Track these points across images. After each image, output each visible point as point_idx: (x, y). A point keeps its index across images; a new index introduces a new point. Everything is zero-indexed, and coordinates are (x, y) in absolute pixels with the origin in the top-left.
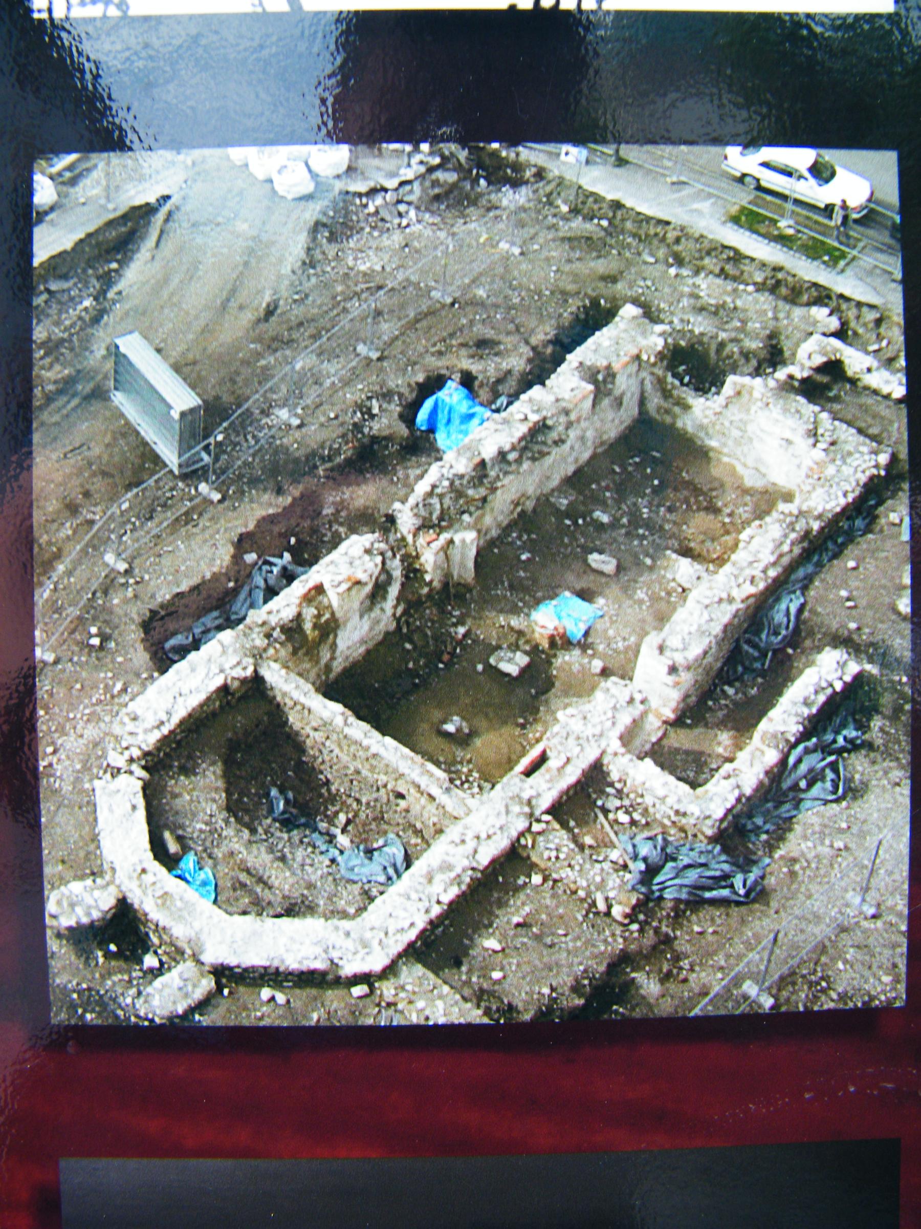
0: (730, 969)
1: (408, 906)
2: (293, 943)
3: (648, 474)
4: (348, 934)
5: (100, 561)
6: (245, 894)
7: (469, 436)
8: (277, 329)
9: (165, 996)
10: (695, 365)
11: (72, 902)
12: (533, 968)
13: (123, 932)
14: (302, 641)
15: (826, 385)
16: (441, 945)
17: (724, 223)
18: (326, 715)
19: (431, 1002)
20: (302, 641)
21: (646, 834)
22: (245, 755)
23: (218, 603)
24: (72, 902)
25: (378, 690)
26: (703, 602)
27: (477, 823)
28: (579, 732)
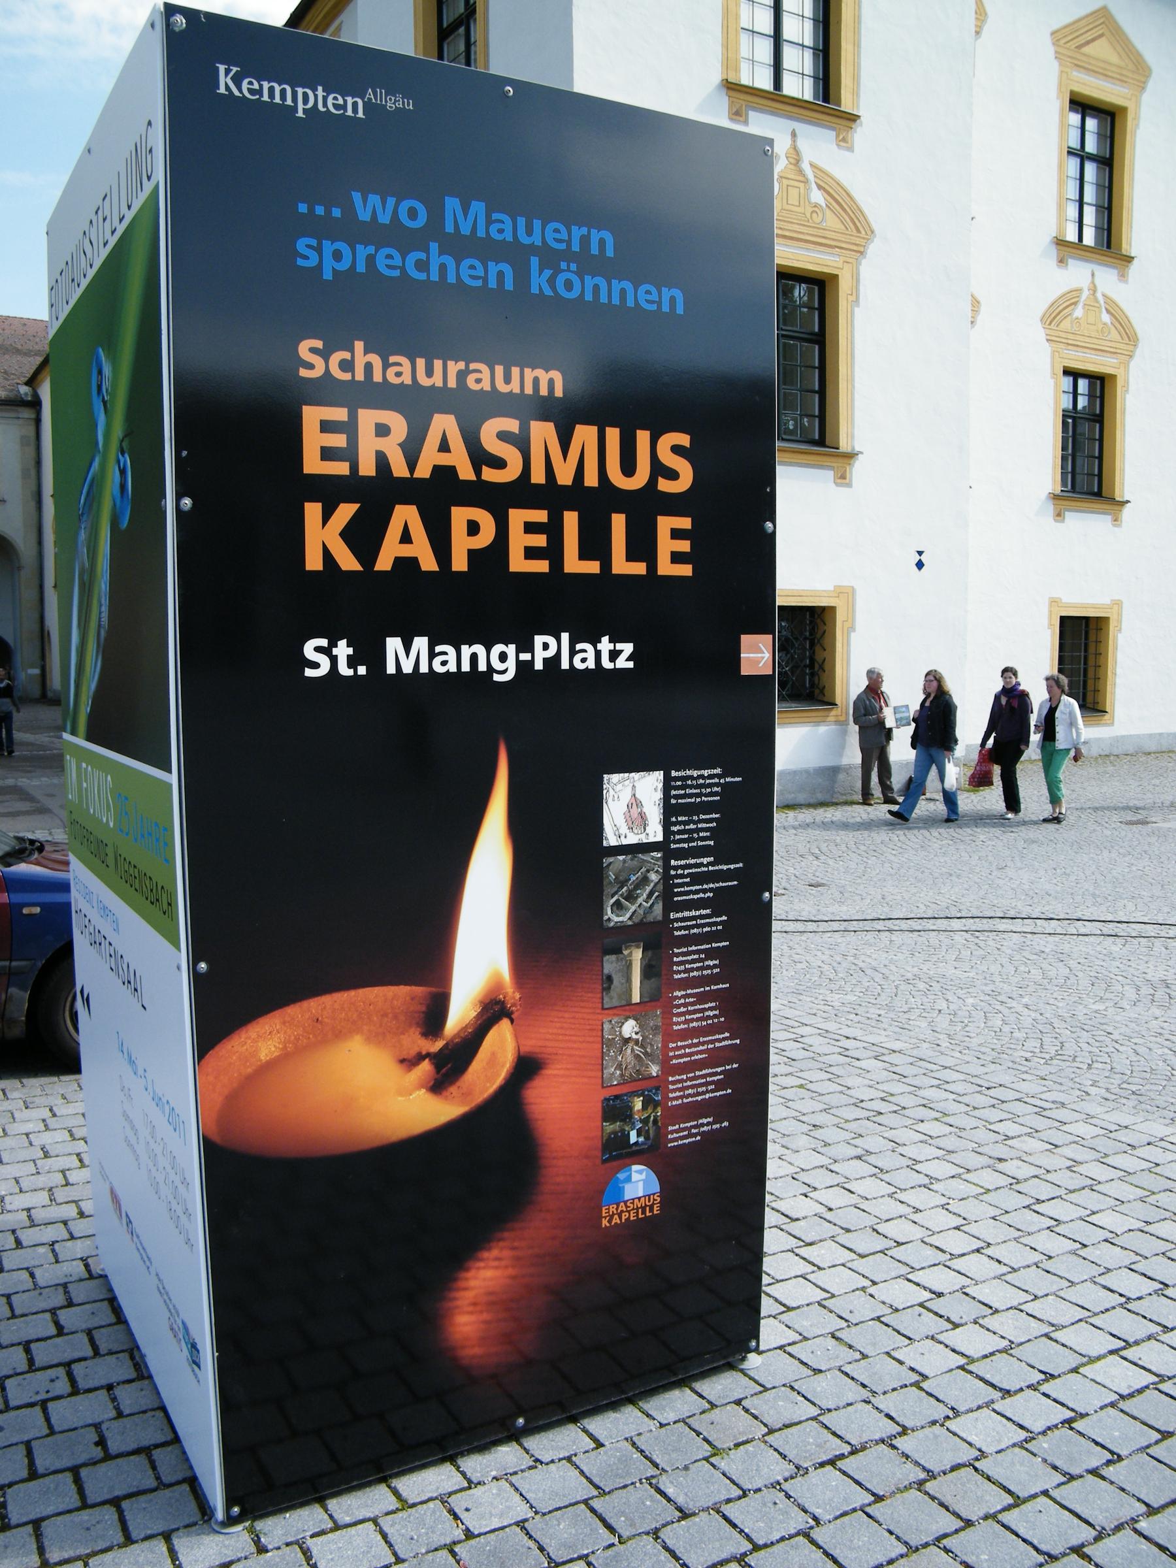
0: (650, 918)
1: (628, 915)
2: (621, 919)
3: (645, 880)
4: (624, 918)
5: (608, 890)
6: (618, 916)
7: (633, 878)
8: (620, 871)
9: (612, 924)
10: (648, 871)
11: (606, 918)
12: (636, 920)
13: (609, 919)
14: (622, 895)
15: (657, 872)
16: (630, 918)
17: (1059, 515)
18: (844, 908)
19: (630, 923)
20: (622, 895)
21: (944, 948)
22: (618, 906)
23: (616, 893)
24: (606, 918)
25: (626, 899)
26: (648, 889)
27: (633, 908)
28: (640, 900)
